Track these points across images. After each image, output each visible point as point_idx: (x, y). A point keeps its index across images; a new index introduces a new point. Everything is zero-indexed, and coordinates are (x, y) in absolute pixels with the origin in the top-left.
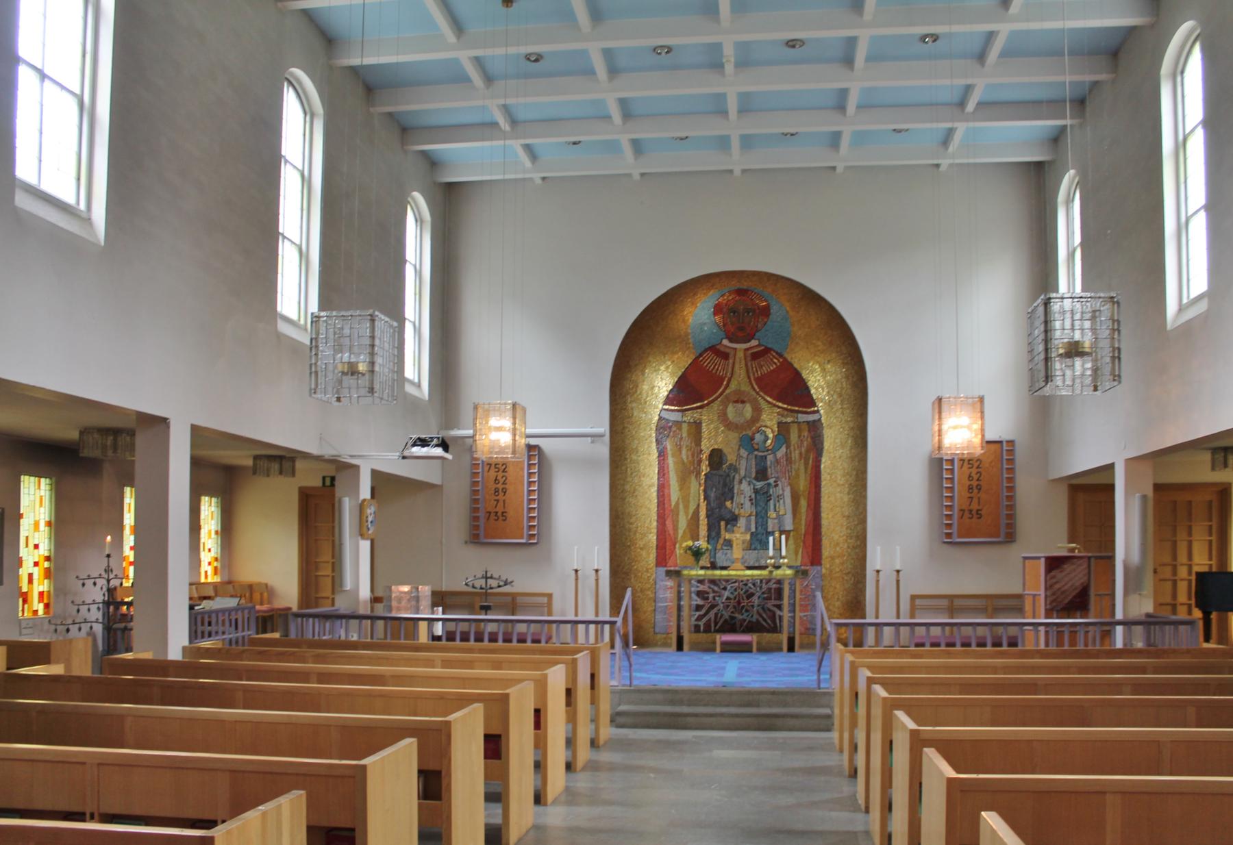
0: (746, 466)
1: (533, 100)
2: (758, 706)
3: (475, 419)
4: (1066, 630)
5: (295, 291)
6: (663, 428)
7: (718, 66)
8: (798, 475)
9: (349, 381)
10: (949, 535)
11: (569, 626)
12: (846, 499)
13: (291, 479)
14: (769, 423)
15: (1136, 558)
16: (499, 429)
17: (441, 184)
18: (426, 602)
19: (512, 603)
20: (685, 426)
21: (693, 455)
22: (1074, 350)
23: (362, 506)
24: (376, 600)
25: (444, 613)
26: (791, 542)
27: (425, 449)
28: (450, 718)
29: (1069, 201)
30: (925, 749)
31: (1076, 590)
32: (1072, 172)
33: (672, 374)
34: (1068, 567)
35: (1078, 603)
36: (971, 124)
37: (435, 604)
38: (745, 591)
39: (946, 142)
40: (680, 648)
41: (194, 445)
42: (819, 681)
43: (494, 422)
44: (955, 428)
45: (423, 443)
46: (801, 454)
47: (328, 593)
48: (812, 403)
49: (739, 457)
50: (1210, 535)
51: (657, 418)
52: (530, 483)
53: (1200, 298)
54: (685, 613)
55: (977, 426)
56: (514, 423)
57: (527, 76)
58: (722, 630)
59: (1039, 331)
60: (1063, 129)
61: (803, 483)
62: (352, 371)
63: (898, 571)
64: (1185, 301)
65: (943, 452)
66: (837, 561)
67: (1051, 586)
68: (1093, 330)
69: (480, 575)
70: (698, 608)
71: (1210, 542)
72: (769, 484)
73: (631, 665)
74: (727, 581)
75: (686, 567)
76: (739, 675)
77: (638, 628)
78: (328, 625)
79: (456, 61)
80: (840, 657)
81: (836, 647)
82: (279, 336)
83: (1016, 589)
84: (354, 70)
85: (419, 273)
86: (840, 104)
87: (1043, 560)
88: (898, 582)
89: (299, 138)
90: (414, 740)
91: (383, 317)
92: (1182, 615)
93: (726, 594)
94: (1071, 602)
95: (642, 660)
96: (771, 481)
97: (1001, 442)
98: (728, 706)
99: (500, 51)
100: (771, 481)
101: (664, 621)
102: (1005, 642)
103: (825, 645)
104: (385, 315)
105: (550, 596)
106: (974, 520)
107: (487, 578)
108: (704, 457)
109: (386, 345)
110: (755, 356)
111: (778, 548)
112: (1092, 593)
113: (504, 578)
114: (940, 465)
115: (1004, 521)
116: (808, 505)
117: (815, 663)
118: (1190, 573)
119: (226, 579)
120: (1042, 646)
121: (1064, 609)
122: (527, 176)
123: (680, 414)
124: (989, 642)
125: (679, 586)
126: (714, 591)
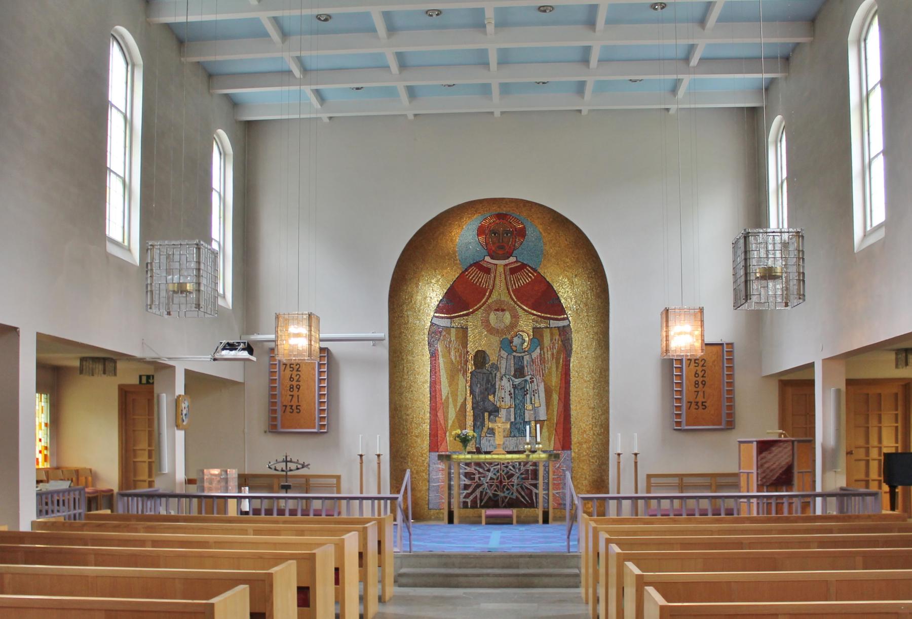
0: (506, 365)
1: (321, 53)
2: (518, 567)
3: (277, 327)
4: (773, 501)
5: (121, 218)
6: (435, 332)
7: (480, 26)
8: (550, 373)
9: (178, 298)
10: (679, 424)
11: (357, 501)
12: (591, 393)
13: (113, 378)
15: (831, 442)
16: (298, 335)
17: (241, 122)
18: (233, 483)
19: (306, 484)
20: (453, 331)
21: (460, 357)
22: (769, 275)
23: (177, 401)
24: (190, 481)
25: (250, 492)
26: (545, 430)
27: (233, 352)
28: (272, 571)
29: (777, 141)
30: (647, 588)
31: (782, 470)
32: (778, 118)
34: (775, 450)
35: (784, 479)
36: (692, 76)
38: (506, 473)
39: (674, 90)
40: (451, 521)
41: (39, 349)
42: (569, 546)
43: (293, 329)
44: (680, 334)
45: (231, 347)
46: (553, 354)
47: (145, 477)
48: (562, 311)
50: (897, 422)
52: (320, 380)
53: (880, 226)
54: (455, 491)
55: (698, 333)
56: (310, 331)
57: (317, 33)
60: (772, 81)
61: (555, 380)
62: (181, 289)
63: (636, 454)
64: (869, 228)
67: (762, 465)
69: (280, 459)
70: (466, 487)
71: (897, 427)
72: (526, 381)
73: (410, 534)
74: (490, 464)
75: (455, 452)
76: (501, 543)
77: (415, 504)
78: (149, 503)
79: (257, 21)
80: (585, 524)
82: (108, 256)
83: (734, 470)
84: (169, 27)
85: (223, 200)
86: (584, 58)
88: (636, 463)
89: (123, 87)
90: (295, 561)
92: (873, 487)
93: (490, 475)
95: (419, 532)
96: (528, 378)
97: (722, 344)
98: (492, 568)
99: (297, 12)
100: (528, 378)
101: (437, 499)
102: (723, 512)
103: (574, 518)
106: (700, 410)
107: (287, 462)
108: (470, 358)
110: (513, 271)
112: (796, 470)
114: (671, 365)
115: (725, 411)
116: (560, 399)
117: (566, 533)
118: (880, 455)
119: (55, 465)
120: (755, 514)
122: (319, 115)
124: (710, 512)
125: (450, 468)
126: (479, 473)
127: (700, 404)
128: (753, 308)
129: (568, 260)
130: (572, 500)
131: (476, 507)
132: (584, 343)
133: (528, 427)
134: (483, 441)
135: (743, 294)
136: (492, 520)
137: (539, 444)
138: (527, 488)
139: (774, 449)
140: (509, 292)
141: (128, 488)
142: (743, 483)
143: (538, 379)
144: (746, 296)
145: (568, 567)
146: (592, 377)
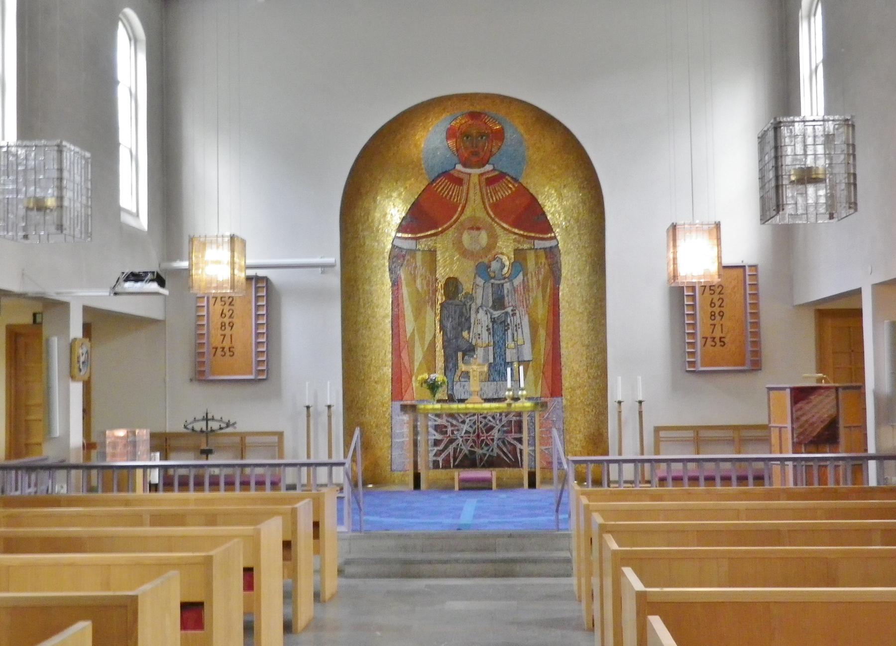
0: (482, 294)
6: (397, 256)
8: (536, 305)
10: (692, 364)
12: (585, 328)
14: (504, 251)
15: (886, 388)
16: (218, 262)
18: (143, 447)
19: (241, 445)
20: (419, 256)
21: (428, 285)
22: (807, 177)
24: (89, 446)
27: (139, 284)
33: (405, 201)
34: (815, 399)
35: (828, 436)
37: (153, 449)
38: (483, 427)
45: (136, 277)
48: (548, 228)
49: (475, 285)
51: (389, 246)
54: (421, 449)
56: (233, 257)
58: (461, 465)
59: (769, 156)
61: (542, 312)
62: (40, 207)
63: (640, 402)
65: (679, 280)
66: (578, 392)
67: (798, 418)
68: (828, 156)
70: (437, 443)
72: (507, 313)
75: (422, 401)
78: (33, 476)
81: (573, 484)
83: (766, 422)
87: (788, 391)
88: (640, 413)
91: (72, 147)
93: (465, 427)
94: (819, 435)
97: (743, 267)
98: (462, 551)
100: (509, 310)
103: (564, 480)
104: (75, 144)
105: (280, 435)
108: (440, 285)
109: (78, 178)
110: (491, 181)
111: (515, 380)
113: (226, 420)
114: (680, 295)
121: (811, 442)
123: (414, 242)
126: (452, 425)
127: (717, 340)
128: (786, 221)
129: (555, 168)
130: (560, 463)
131: (450, 467)
132: (576, 267)
133: (509, 370)
134: (457, 387)
135: (772, 202)
136: (467, 485)
137: (522, 390)
138: (510, 443)
139: (812, 397)
140: (485, 208)
141: (18, 455)
142: (774, 439)
143: (521, 311)
144: (778, 206)
145: (557, 550)
146: (586, 309)
